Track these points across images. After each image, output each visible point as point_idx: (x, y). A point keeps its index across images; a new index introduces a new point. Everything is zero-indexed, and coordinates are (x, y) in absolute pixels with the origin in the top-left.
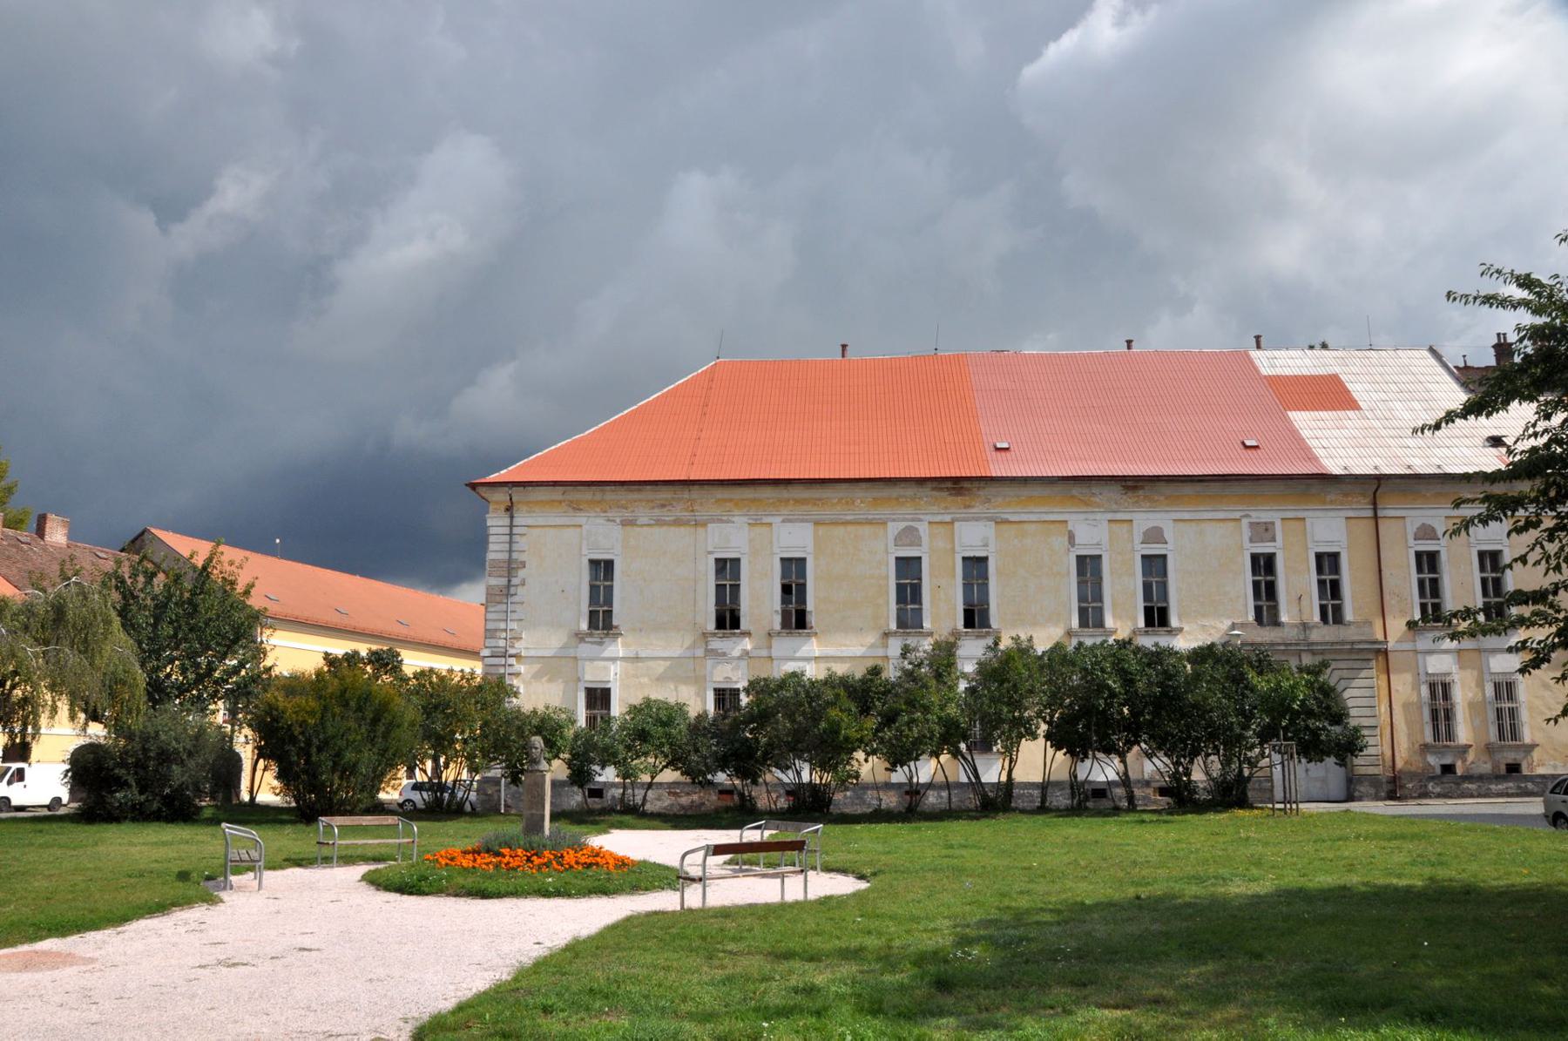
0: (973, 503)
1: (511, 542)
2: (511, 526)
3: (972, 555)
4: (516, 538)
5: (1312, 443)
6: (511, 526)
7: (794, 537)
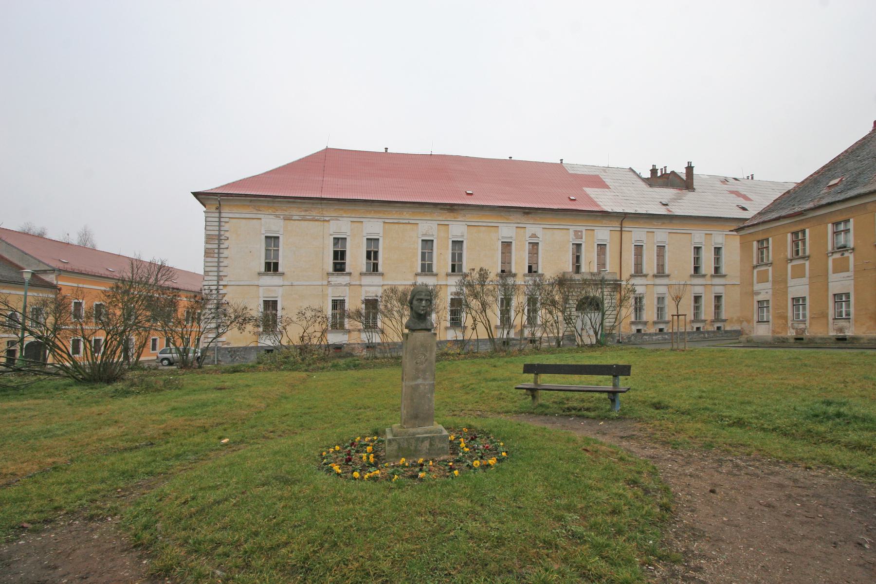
1: (220, 226)
2: (220, 217)
4: (223, 224)
5: (596, 200)
6: (220, 217)
7: (373, 226)
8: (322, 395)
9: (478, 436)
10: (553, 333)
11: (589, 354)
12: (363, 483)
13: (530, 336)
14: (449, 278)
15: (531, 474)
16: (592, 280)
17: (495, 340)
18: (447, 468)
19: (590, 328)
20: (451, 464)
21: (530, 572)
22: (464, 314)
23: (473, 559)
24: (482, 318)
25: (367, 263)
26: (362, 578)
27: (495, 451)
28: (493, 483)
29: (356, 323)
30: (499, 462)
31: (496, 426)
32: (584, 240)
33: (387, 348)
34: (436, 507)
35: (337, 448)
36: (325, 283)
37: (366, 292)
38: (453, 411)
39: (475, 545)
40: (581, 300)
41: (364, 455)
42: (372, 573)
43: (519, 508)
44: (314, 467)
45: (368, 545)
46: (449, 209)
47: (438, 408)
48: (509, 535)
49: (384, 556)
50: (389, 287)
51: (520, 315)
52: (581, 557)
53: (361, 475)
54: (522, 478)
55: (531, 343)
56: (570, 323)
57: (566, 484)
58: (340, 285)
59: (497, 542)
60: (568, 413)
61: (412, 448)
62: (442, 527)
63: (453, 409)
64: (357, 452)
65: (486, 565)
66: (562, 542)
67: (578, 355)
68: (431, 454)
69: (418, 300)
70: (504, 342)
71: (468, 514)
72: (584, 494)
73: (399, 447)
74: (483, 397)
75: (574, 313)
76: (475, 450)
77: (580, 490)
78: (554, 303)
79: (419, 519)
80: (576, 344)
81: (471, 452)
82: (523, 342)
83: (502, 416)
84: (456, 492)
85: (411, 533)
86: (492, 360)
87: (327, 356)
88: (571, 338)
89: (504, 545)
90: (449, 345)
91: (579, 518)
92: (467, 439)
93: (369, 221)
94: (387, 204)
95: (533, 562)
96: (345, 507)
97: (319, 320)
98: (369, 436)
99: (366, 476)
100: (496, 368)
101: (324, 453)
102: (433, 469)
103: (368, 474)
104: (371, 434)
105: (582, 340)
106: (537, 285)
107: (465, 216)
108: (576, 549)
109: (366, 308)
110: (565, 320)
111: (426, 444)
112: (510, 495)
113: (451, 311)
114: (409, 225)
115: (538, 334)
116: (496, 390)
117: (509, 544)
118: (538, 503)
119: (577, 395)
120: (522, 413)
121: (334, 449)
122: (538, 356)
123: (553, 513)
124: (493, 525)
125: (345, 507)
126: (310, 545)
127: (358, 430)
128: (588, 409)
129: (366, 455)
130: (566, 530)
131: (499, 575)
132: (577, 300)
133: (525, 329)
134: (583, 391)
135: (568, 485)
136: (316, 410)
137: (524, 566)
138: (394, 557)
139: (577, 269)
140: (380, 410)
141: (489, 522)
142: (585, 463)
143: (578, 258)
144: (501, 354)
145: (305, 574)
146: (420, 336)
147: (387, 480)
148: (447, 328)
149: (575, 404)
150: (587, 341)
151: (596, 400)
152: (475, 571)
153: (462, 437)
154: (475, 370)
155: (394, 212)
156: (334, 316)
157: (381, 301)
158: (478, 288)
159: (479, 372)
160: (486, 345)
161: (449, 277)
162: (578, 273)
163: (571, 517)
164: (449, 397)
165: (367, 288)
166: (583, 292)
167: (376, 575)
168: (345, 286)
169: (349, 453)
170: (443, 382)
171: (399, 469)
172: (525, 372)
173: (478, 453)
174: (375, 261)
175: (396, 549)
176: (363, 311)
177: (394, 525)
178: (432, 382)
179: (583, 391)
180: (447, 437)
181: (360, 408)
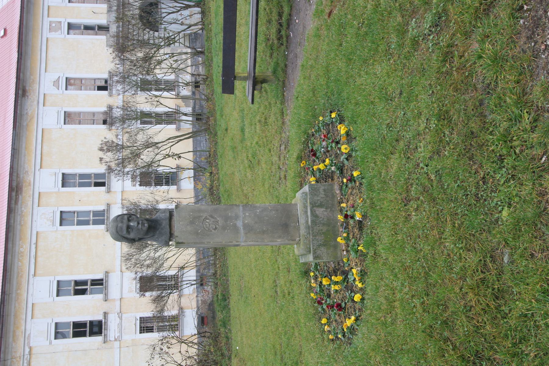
0: (28, 181)
3: (61, 182)
8: (260, 338)
9: (311, 148)
10: (186, 59)
11: (213, 15)
12: (368, 289)
13: (190, 88)
14: (112, 189)
15: (359, 81)
16: (117, 11)
17: (195, 130)
18: (350, 185)
19: (181, 15)
20: (345, 180)
21: (481, 78)
22: (160, 169)
23: (465, 149)
24: (165, 147)
25: (91, 293)
26: (488, 287)
27: (330, 126)
28: (370, 127)
29: (170, 301)
30: (344, 121)
31: (300, 126)
32: (62, 20)
33: (202, 261)
34: (399, 197)
35: (324, 321)
36: (117, 344)
37: (130, 291)
38: (280, 179)
39: (447, 148)
40: (144, 24)
41: (333, 288)
42: (482, 276)
43: (401, 94)
44: (348, 350)
45: (447, 281)
46: (17, 192)
47: (277, 197)
48: (435, 105)
49: (461, 262)
50: (123, 264)
51: (162, 101)
52: (463, 15)
53: (358, 292)
54: (364, 91)
55: (198, 87)
56: (174, 38)
57: (372, 37)
58: (120, 325)
59: (444, 120)
60: (285, 39)
61: (325, 229)
62: (425, 190)
63: (278, 178)
64: (329, 296)
65: (472, 133)
66: (444, 40)
67: (213, 29)
68: (333, 205)
69: (128, 232)
70: (197, 119)
71: (409, 158)
72: (385, 14)
73: (324, 245)
74: (263, 143)
75: (162, 33)
76: (328, 151)
77: (379, 20)
78: (147, 59)
79: (414, 218)
80: (200, 32)
81: (330, 156)
82: (197, 96)
83: (287, 119)
84: (380, 173)
85: (432, 228)
86: (219, 133)
87: (211, 334)
88: (193, 38)
89: (447, 112)
90: (200, 186)
91: (414, 20)
92: (314, 161)
93: (32, 295)
94: (8, 274)
95: (469, 74)
96: (399, 311)
97: (165, 348)
98: (310, 282)
99: (360, 285)
100: (229, 128)
101: (331, 337)
102: (351, 202)
103: (357, 283)
104: (308, 279)
105: (196, 25)
106: (124, 78)
107: (27, 172)
108: (453, 21)
109: (151, 290)
110: (169, 45)
111: (320, 211)
112: (385, 106)
113: (156, 184)
114: (39, 244)
115: (188, 78)
116: (255, 128)
117: (447, 105)
118: (396, 70)
119: (262, 28)
120: (284, 95)
121: (325, 324)
122: (214, 77)
123: (409, 52)
124: (422, 125)
125: (399, 311)
126: (446, 355)
127: (302, 296)
128: (280, 15)
129: (333, 286)
130: (429, 35)
131: (485, 116)
132: (144, 30)
133: (181, 94)
134: (257, 20)
135: (373, 34)
136: (278, 347)
137: (474, 85)
138: (462, 248)
139: (103, 29)
140: (279, 267)
141: (418, 131)
142: (346, 14)
143: (88, 28)
144: (212, 122)
145: (482, 360)
146: (178, 226)
147: (364, 261)
148: (179, 190)
149: (274, 31)
150: (197, 18)
151: (268, 5)
152: (481, 146)
153: (312, 167)
154: (230, 153)
155: (20, 264)
156: (160, 329)
157: (142, 272)
158: (126, 152)
159: (234, 148)
160: (200, 142)
161: (112, 190)
162: (108, 28)
163: (413, 30)
164: (263, 185)
165: (125, 291)
166: (133, 22)
167: (484, 271)
168: (121, 318)
169: (331, 307)
170: (245, 191)
171: (351, 244)
172: (232, 93)
173: (331, 147)
174: (89, 283)
175: (452, 246)
176: (155, 293)
177: (421, 250)
178: (241, 208)
179: (257, 20)
180: (311, 186)
181: (276, 292)
